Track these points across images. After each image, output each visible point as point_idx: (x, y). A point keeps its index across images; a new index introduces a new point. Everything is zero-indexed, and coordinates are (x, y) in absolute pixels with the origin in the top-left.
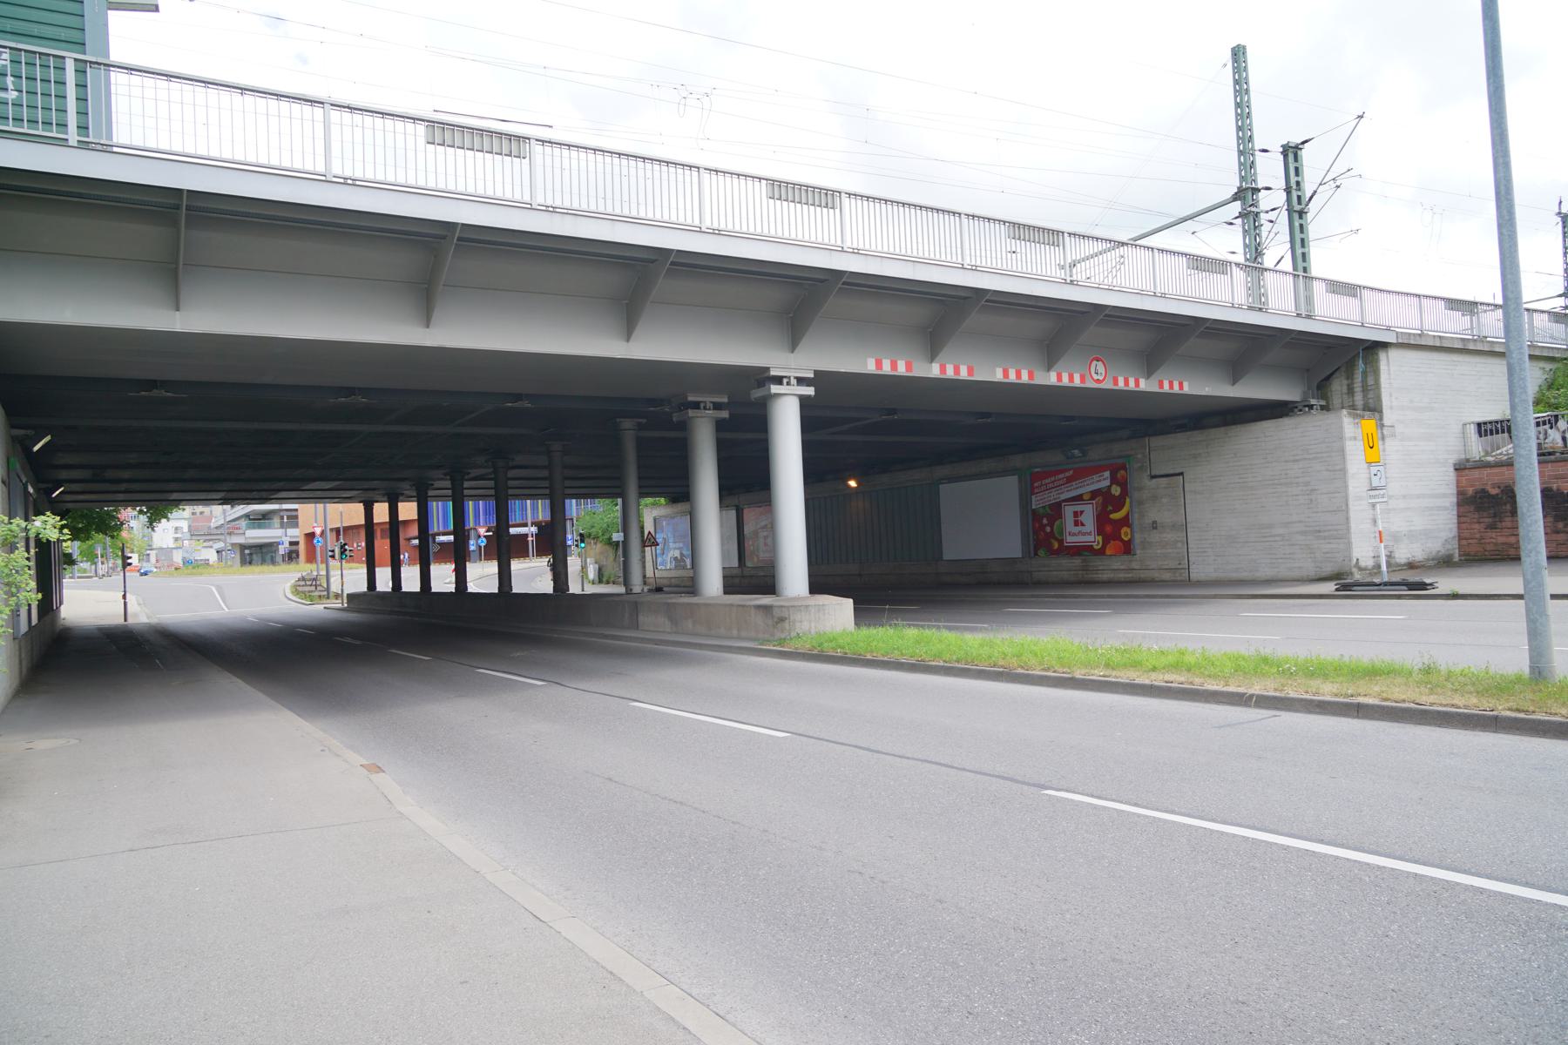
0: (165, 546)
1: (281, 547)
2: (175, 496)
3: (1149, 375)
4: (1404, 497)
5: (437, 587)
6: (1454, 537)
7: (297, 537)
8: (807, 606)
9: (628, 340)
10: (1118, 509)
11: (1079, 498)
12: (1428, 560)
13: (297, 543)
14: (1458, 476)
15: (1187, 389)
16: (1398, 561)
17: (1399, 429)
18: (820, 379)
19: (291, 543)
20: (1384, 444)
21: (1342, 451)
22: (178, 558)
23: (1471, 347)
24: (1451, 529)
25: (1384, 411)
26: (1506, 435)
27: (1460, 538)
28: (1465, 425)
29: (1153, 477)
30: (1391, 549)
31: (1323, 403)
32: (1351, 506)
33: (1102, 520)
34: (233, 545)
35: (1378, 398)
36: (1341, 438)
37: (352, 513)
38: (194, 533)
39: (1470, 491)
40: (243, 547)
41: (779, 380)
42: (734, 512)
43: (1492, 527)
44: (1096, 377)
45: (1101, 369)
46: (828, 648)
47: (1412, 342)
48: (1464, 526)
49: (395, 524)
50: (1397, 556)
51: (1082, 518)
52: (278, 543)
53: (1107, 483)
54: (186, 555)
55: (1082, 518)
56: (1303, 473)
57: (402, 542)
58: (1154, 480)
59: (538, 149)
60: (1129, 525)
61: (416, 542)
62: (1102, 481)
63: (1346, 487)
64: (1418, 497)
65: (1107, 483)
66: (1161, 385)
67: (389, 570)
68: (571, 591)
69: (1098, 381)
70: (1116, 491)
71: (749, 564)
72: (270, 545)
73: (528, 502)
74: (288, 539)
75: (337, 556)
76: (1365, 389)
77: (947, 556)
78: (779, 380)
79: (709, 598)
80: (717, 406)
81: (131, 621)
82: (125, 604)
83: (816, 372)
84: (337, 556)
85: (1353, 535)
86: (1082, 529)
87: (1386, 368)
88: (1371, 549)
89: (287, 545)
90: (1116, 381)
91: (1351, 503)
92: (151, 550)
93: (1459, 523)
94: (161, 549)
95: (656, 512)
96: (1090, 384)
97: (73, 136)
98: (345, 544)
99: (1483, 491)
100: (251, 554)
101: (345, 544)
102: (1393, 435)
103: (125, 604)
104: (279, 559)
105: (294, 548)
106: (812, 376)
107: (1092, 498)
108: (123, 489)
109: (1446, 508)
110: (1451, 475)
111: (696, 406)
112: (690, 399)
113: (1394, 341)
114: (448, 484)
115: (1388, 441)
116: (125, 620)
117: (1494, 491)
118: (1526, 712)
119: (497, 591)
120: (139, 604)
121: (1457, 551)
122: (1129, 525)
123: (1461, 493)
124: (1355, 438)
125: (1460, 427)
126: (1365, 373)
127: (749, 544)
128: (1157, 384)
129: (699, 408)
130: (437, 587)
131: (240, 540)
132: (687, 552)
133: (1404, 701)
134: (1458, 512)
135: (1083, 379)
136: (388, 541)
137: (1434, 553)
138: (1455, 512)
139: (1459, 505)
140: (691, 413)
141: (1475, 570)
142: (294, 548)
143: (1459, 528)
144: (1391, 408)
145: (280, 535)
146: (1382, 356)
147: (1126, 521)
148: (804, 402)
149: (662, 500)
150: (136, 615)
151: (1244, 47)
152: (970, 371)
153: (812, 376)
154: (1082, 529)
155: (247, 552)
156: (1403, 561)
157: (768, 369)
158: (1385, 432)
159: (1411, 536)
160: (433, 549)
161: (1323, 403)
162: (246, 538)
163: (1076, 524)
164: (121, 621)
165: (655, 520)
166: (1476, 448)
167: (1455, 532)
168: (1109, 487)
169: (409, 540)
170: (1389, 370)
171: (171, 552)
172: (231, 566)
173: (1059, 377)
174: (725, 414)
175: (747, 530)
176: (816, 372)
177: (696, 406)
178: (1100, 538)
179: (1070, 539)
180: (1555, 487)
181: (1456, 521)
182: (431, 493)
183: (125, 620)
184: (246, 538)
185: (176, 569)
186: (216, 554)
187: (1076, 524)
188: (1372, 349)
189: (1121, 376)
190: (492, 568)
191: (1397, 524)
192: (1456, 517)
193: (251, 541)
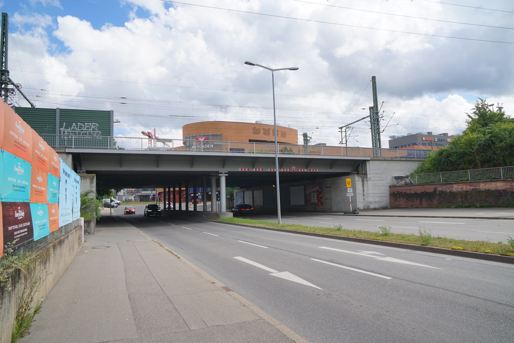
0: (120, 195)
1: (150, 196)
2: (122, 187)
3: (307, 169)
4: (373, 194)
5: (190, 209)
6: (388, 203)
7: (155, 193)
8: (222, 214)
9: (192, 168)
10: (320, 195)
11: (314, 192)
12: (380, 208)
13: (155, 195)
14: (390, 189)
15: (317, 170)
16: (371, 208)
17: (372, 179)
18: (229, 173)
19: (153, 195)
20: (367, 182)
21: (355, 184)
22: (124, 198)
23: (394, 159)
24: (387, 201)
25: (368, 175)
26: (400, 180)
27: (390, 203)
28: (392, 177)
29: (326, 187)
30: (369, 205)
31: (357, 172)
32: (357, 196)
33: (318, 197)
34: (138, 195)
35: (367, 172)
36: (355, 181)
37: (161, 190)
38: (128, 192)
39: (392, 192)
40: (141, 196)
41: (221, 173)
42: (252, 192)
43: (395, 201)
44: (293, 169)
45: (294, 168)
46: (317, 232)
47: (375, 159)
48: (391, 200)
49: (180, 191)
50: (370, 207)
51: (314, 196)
52: (150, 195)
53: (318, 188)
54: (126, 198)
55: (314, 196)
56: (479, 175)
57: (182, 196)
58: (327, 188)
59: (174, 141)
60: (322, 198)
61: (185, 196)
62: (317, 188)
63: (356, 192)
64: (377, 193)
65: (318, 188)
66: (310, 170)
67: (178, 204)
68: (176, 209)
69: (294, 170)
70: (320, 190)
71: (255, 205)
72: (148, 195)
73: (200, 188)
74: (152, 194)
75: (158, 201)
76: (364, 170)
77: (292, 204)
78: (221, 173)
79: (214, 212)
80: (225, 173)
81: (112, 215)
82: (111, 211)
83: (228, 171)
84: (158, 201)
85: (357, 202)
86: (315, 200)
87: (369, 165)
88: (363, 205)
89: (152, 196)
90: (298, 170)
91: (357, 195)
92: (117, 196)
93: (390, 200)
94: (120, 195)
95: (236, 191)
96: (291, 171)
97: (109, 147)
98: (160, 198)
99: (394, 192)
100: (143, 198)
101: (160, 198)
102: (370, 180)
103: (111, 211)
104: (150, 200)
105: (154, 197)
106: (228, 172)
107: (316, 192)
108: (119, 212)
109: (386, 196)
110: (388, 188)
111: (212, 176)
112: (211, 174)
113: (370, 159)
114: (178, 185)
115: (369, 182)
116: (111, 215)
117: (396, 193)
118: (392, 242)
119: (178, 210)
120: (114, 211)
121: (389, 206)
122: (322, 198)
123: (390, 193)
124: (359, 181)
125: (391, 177)
126: (364, 166)
127: (255, 201)
128: (309, 170)
129: (212, 176)
130: (190, 209)
131: (140, 194)
132: (243, 201)
133: (374, 239)
134: (390, 197)
135: (290, 170)
136: (178, 195)
137: (382, 206)
138: (389, 197)
139: (390, 195)
140: (211, 177)
141: (393, 210)
142: (154, 197)
143: (390, 201)
144: (370, 174)
145: (150, 193)
146: (368, 163)
147: (321, 198)
148: (226, 177)
149: (239, 188)
150: (113, 214)
151: (375, 77)
152: (262, 170)
153: (228, 172)
154: (315, 200)
155: (142, 197)
156: (372, 208)
157: (219, 171)
158: (368, 179)
159: (375, 202)
160: (189, 198)
161: (357, 172)
162: (141, 194)
163: (313, 198)
164: (110, 215)
165: (236, 193)
166: (395, 182)
167: (389, 201)
168: (319, 189)
169: (184, 195)
170: (369, 166)
171: (122, 197)
172: (136, 202)
173: (284, 170)
174: (227, 175)
175: (255, 196)
176: (228, 171)
177: (212, 176)
178: (317, 201)
179: (313, 201)
180: (406, 192)
181: (389, 199)
182: (182, 186)
183: (111, 215)
184: (141, 194)
185: (123, 202)
186: (134, 198)
187: (313, 198)
188: (364, 162)
189: (302, 169)
190: (202, 204)
191: (371, 199)
192: (389, 198)
193: (143, 194)
